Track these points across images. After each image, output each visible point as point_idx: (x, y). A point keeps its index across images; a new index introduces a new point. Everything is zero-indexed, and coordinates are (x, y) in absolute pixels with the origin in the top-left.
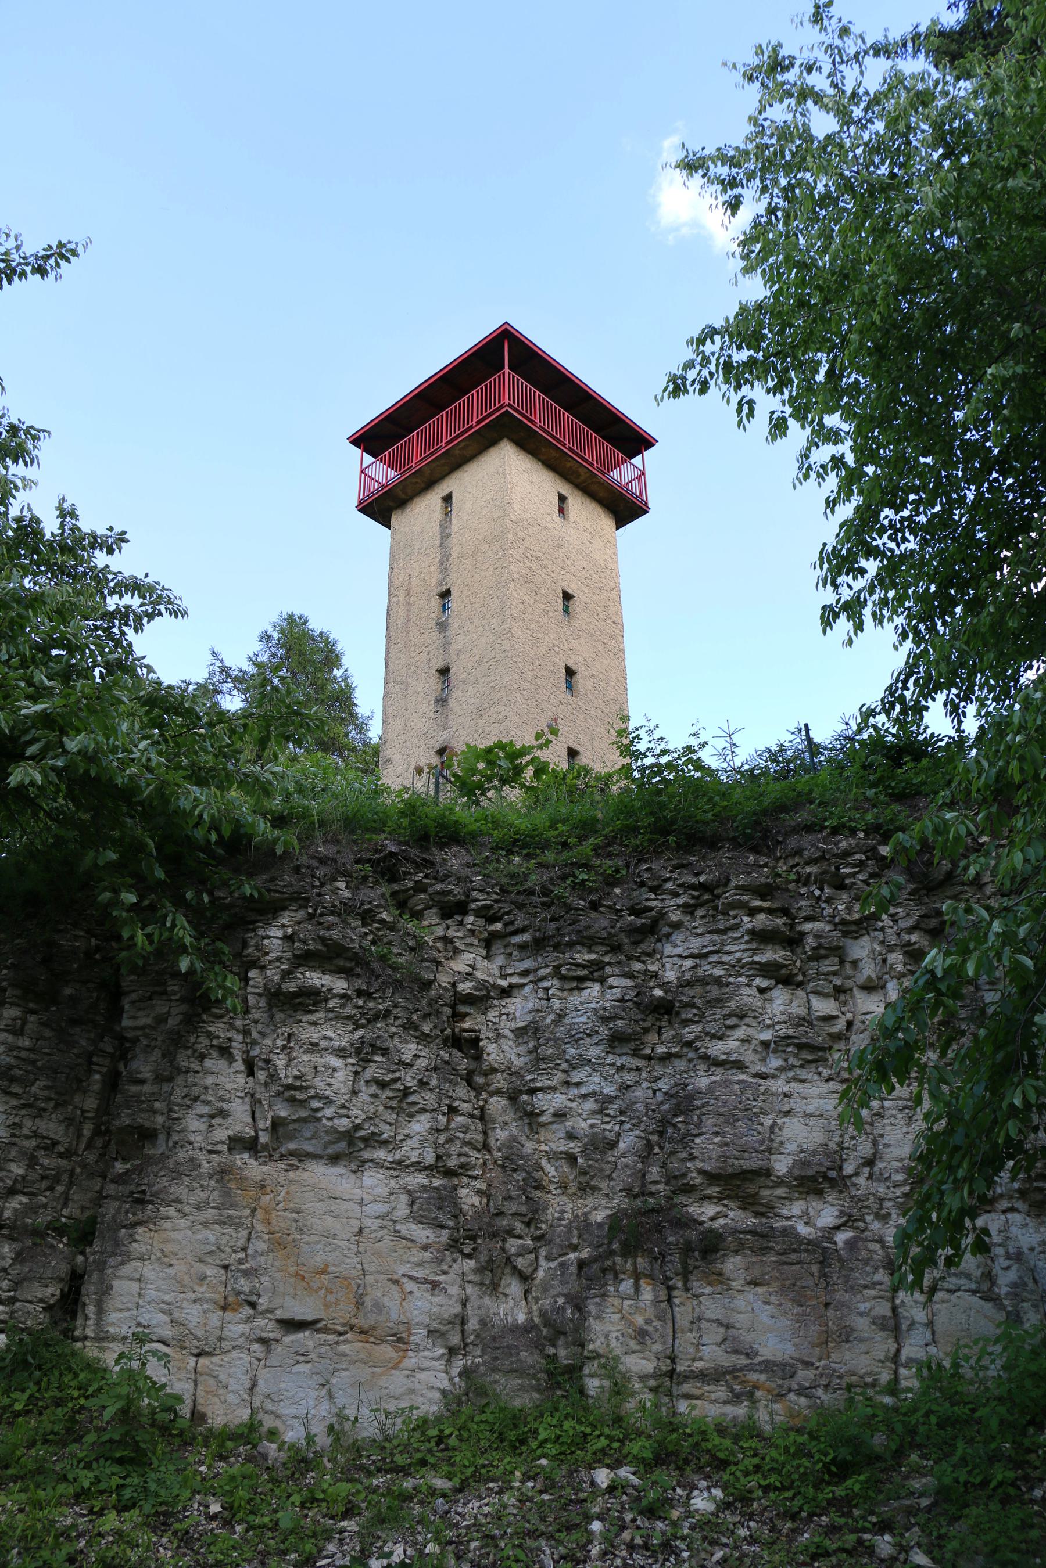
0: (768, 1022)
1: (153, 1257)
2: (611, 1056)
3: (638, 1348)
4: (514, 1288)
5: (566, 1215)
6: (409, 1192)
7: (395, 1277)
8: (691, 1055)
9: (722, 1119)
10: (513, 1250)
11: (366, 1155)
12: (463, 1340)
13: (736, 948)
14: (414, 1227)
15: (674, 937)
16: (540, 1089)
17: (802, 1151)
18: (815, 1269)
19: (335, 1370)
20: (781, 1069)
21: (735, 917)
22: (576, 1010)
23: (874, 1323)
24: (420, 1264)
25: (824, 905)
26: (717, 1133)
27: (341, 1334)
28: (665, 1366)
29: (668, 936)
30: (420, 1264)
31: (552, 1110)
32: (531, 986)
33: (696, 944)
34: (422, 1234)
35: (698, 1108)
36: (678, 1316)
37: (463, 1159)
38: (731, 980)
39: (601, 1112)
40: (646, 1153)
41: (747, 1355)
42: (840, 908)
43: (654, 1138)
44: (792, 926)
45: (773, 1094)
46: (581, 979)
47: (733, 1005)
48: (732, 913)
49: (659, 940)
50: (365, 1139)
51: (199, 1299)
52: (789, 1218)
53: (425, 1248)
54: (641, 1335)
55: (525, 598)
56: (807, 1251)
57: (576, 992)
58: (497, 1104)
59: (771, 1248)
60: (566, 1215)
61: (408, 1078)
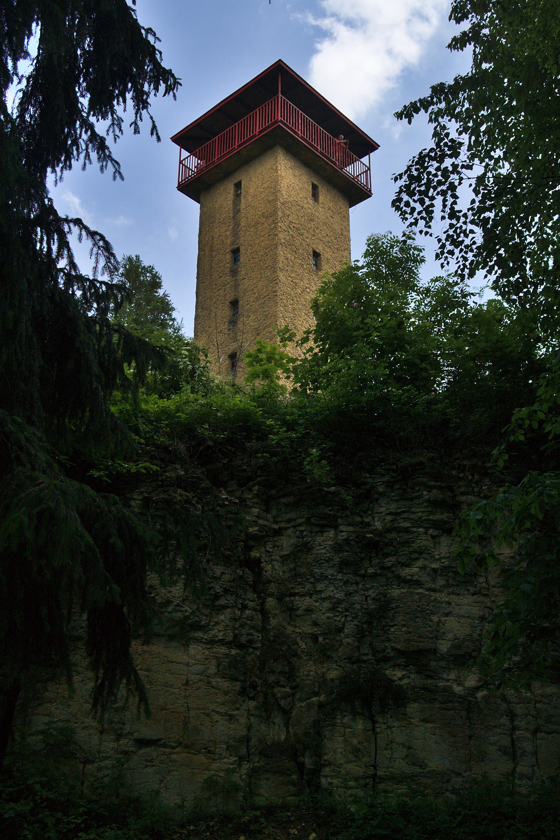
0: (437, 557)
1: (58, 701)
2: (340, 575)
3: (354, 759)
4: (278, 719)
5: (311, 673)
6: (217, 658)
7: (207, 712)
8: (389, 575)
9: (408, 616)
10: (279, 695)
11: (192, 635)
12: (248, 751)
13: (418, 510)
14: (219, 680)
15: (380, 501)
16: (297, 594)
17: (456, 639)
18: (463, 713)
19: (170, 771)
20: (444, 586)
21: (418, 491)
22: (320, 545)
23: (499, 750)
24: (223, 704)
25: (473, 485)
26: (404, 625)
27: (173, 748)
28: (371, 772)
29: (377, 500)
30: (223, 704)
31: (304, 607)
32: (292, 529)
33: (393, 507)
34: (225, 684)
35: (393, 609)
36: (378, 739)
37: (250, 637)
38: (415, 529)
39: (333, 609)
40: (360, 634)
41: (421, 766)
42: (484, 488)
43: (365, 626)
44: (454, 497)
45: (439, 602)
46: (323, 526)
47: (415, 546)
48: (416, 488)
49: (371, 502)
50: (191, 626)
51: (86, 727)
52: (448, 680)
53: (226, 693)
54: (356, 751)
55: (289, 255)
56: (459, 702)
57: (319, 534)
58: (271, 602)
59: (436, 699)
60: (311, 673)
61: (218, 587)
